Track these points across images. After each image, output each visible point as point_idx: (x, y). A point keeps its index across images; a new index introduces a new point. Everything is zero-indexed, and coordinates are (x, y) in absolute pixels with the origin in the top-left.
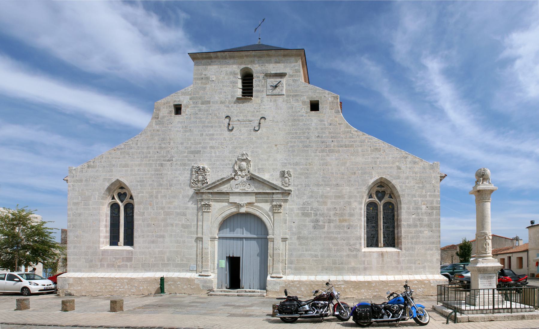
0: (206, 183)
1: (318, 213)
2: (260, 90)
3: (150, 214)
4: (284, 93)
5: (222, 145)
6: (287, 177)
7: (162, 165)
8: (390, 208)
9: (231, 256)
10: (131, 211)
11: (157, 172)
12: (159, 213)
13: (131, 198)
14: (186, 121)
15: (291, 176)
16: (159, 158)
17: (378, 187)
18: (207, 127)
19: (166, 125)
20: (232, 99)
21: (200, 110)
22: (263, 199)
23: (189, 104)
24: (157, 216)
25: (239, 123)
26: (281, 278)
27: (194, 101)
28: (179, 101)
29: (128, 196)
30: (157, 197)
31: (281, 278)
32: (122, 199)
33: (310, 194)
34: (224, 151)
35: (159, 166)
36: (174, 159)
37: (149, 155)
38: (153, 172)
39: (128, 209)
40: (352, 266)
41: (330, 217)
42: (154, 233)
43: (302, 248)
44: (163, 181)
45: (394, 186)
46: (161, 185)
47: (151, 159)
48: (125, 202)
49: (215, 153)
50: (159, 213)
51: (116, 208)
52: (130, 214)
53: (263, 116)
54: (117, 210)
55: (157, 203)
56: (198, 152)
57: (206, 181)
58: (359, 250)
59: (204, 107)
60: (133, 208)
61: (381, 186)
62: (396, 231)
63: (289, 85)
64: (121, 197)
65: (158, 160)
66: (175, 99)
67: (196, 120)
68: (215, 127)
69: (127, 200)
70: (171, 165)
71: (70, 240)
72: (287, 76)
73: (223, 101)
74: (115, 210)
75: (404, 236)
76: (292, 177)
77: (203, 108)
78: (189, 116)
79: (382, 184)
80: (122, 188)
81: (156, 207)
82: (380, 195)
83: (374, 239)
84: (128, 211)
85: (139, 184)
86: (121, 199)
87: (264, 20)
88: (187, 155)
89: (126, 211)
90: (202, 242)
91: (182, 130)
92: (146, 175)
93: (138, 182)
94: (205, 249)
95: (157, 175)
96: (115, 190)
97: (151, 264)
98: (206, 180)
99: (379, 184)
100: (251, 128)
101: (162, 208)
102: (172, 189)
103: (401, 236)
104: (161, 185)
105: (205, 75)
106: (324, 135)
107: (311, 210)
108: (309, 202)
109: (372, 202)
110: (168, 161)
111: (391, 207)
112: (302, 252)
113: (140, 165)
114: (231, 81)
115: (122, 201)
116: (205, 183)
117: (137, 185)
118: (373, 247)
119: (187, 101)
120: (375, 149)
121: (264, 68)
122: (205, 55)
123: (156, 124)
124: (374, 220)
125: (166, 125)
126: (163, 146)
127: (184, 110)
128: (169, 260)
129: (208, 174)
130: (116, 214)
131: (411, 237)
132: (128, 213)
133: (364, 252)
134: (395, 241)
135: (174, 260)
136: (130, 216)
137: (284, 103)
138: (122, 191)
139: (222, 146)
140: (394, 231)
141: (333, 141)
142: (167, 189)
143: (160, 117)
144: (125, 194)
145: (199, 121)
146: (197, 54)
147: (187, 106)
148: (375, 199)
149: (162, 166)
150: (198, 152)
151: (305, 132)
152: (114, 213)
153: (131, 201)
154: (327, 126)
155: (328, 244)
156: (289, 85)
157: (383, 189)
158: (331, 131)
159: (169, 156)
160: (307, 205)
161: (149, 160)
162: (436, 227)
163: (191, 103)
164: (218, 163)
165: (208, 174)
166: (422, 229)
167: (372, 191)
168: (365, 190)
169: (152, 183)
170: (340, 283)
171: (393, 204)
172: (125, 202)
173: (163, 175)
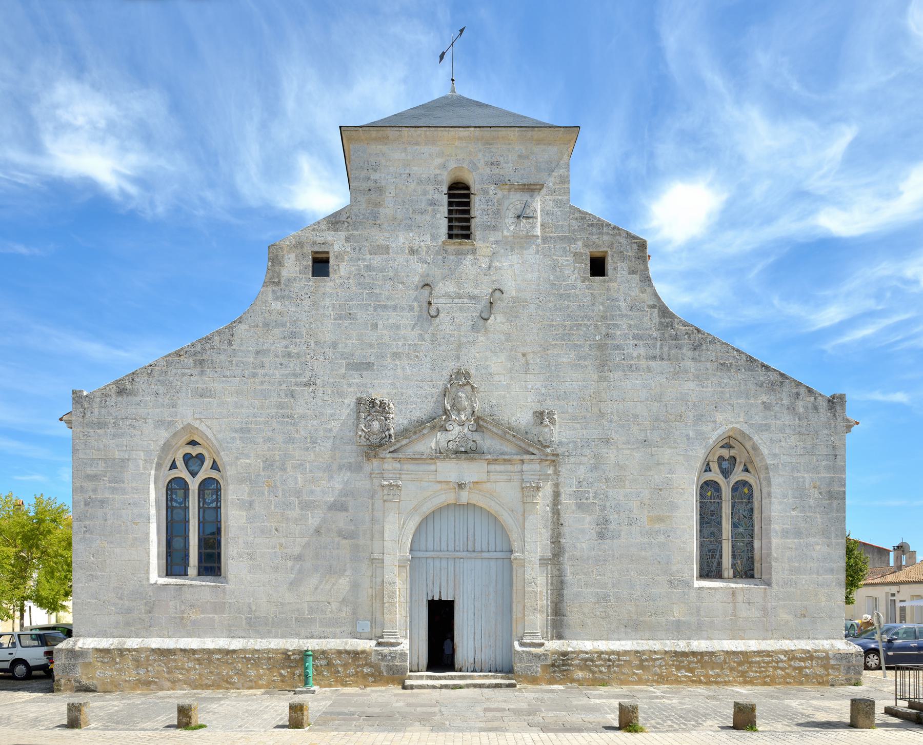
0: (388, 436)
1: (608, 505)
2: (489, 223)
3: (267, 506)
4: (539, 234)
5: (417, 352)
6: (547, 426)
7: (292, 394)
8: (745, 493)
9: (436, 598)
10: (214, 497)
11: (281, 409)
12: (290, 503)
13: (215, 467)
14: (340, 292)
15: (554, 424)
16: (284, 379)
17: (722, 447)
18: (385, 307)
19: (298, 301)
20: (434, 244)
21: (369, 268)
22: (912, 687)
23: (344, 253)
24: (284, 510)
25: (449, 301)
26: (542, 645)
27: (355, 244)
28: (323, 244)
29: (208, 463)
30: (284, 469)
31: (542, 645)
32: (194, 468)
33: (592, 461)
34: (422, 365)
35: (286, 395)
36: (318, 380)
37: (261, 371)
38: (273, 411)
39: (206, 491)
40: (674, 619)
41: (631, 511)
42: (277, 550)
43: (579, 580)
44: (297, 431)
45: (755, 448)
46: (291, 440)
47: (267, 378)
48: (201, 476)
49: (403, 369)
50: (290, 503)
51: (179, 489)
52: (212, 502)
53: (497, 287)
54: (181, 493)
55: (284, 482)
56: (369, 366)
57: (387, 433)
58: (689, 585)
59: (377, 260)
60: (218, 491)
61: (728, 446)
62: (756, 544)
63: (547, 214)
64: (190, 463)
65: (284, 382)
66: (315, 238)
67: (361, 291)
68: (402, 309)
69: (205, 472)
70: (313, 395)
71: (78, 563)
72: (544, 191)
73: (415, 248)
74: (176, 494)
75: (775, 555)
76: (557, 427)
77: (374, 263)
78: (346, 281)
79: (731, 443)
80: (193, 443)
81: (283, 490)
82: (725, 465)
83: (713, 560)
84: (206, 496)
85: (237, 435)
86: (190, 468)
87: (462, 31)
88: (345, 373)
89: (201, 496)
90: (730, 728)
91: (332, 313)
92: (255, 416)
93: (236, 431)
94: (390, 584)
95: (283, 416)
96: (178, 449)
97: (270, 620)
98: (388, 430)
99: (725, 441)
100: (475, 314)
101: (298, 493)
102: (317, 449)
103: (769, 555)
104: (291, 440)
105: (376, 181)
106: (619, 333)
107: (594, 498)
108: (591, 480)
109: (712, 481)
110: (306, 385)
111: (746, 490)
112: (578, 588)
113: (238, 393)
114: (429, 200)
115: (194, 474)
116: (386, 436)
117: (234, 438)
118: (711, 577)
119: (341, 246)
120: (722, 364)
121: (497, 171)
122: (375, 132)
123: (276, 299)
124: (714, 520)
125: (298, 301)
126: (294, 350)
127: (336, 267)
128: (311, 610)
129: (391, 416)
130: (180, 503)
131: (788, 558)
132: (207, 500)
133: (700, 588)
134: (753, 564)
135: (322, 610)
136: (211, 508)
137: (537, 256)
138: (194, 451)
139: (417, 354)
140: (751, 544)
141: (636, 345)
142: (307, 449)
143: (283, 281)
144: (200, 458)
145: (367, 293)
146: (360, 129)
147: (339, 257)
148: (716, 475)
149: (293, 396)
150: (369, 366)
151: (581, 325)
152: (176, 501)
153: (214, 474)
154: (625, 312)
155: (628, 571)
156: (547, 214)
157: (733, 452)
158: (632, 322)
159: (309, 374)
160: (586, 488)
161: (262, 383)
162: (837, 535)
163: (349, 249)
164: (410, 392)
165: (391, 416)
166: (811, 540)
167: (710, 458)
168: (699, 453)
169: (270, 433)
170: (657, 656)
171: (751, 486)
172: (201, 476)
173: (295, 416)
